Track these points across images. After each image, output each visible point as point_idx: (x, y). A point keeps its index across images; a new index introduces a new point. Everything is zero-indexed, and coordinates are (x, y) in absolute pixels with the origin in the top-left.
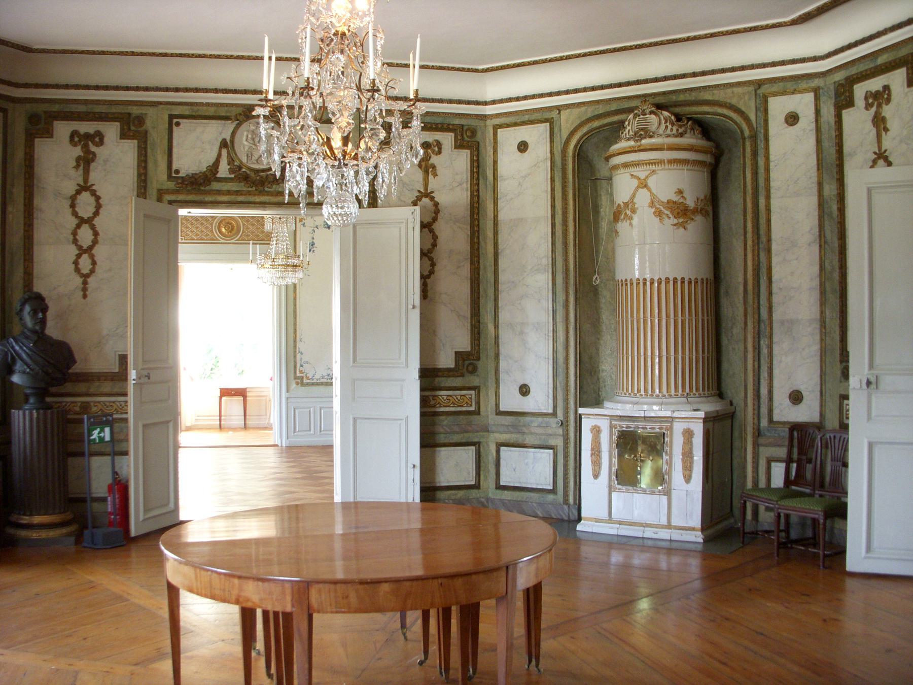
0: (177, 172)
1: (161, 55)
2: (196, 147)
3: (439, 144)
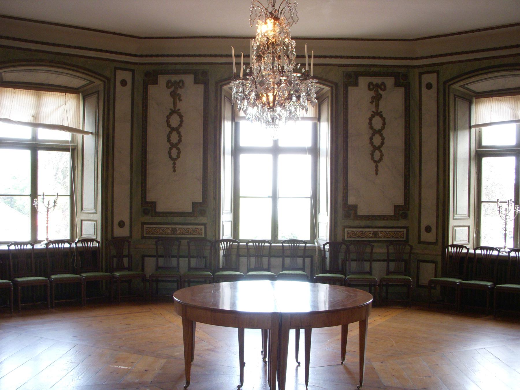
1: (177, 38)
3: (383, 84)
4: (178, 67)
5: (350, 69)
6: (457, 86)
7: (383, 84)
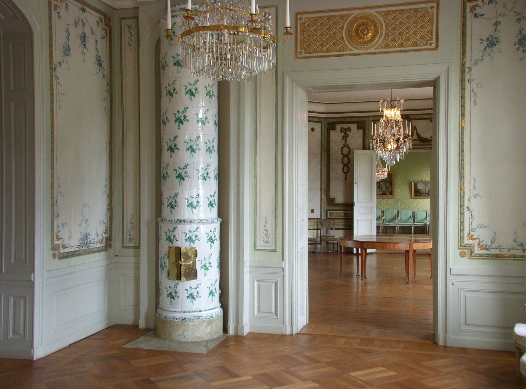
4: (348, 120)
5: (331, 120)
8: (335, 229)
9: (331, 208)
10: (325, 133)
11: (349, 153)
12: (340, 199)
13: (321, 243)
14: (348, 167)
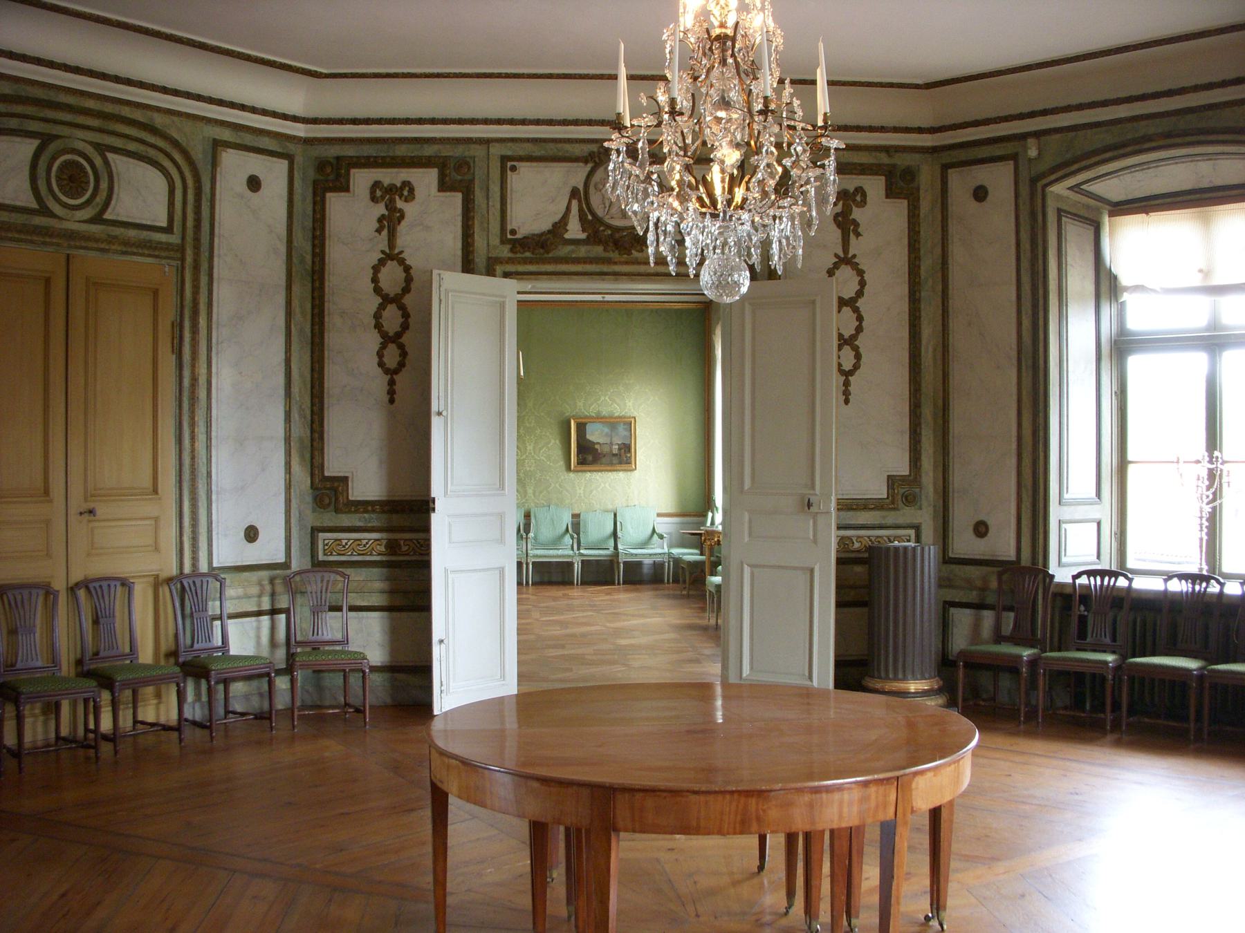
0: (513, 232)
2: (536, 199)
3: (860, 190)
4: (401, 151)
6: (1059, 189)
7: (860, 190)
8: (353, 609)
9: (329, 519)
10: (304, 206)
11: (406, 290)
12: (368, 484)
13: (289, 670)
14: (401, 347)
